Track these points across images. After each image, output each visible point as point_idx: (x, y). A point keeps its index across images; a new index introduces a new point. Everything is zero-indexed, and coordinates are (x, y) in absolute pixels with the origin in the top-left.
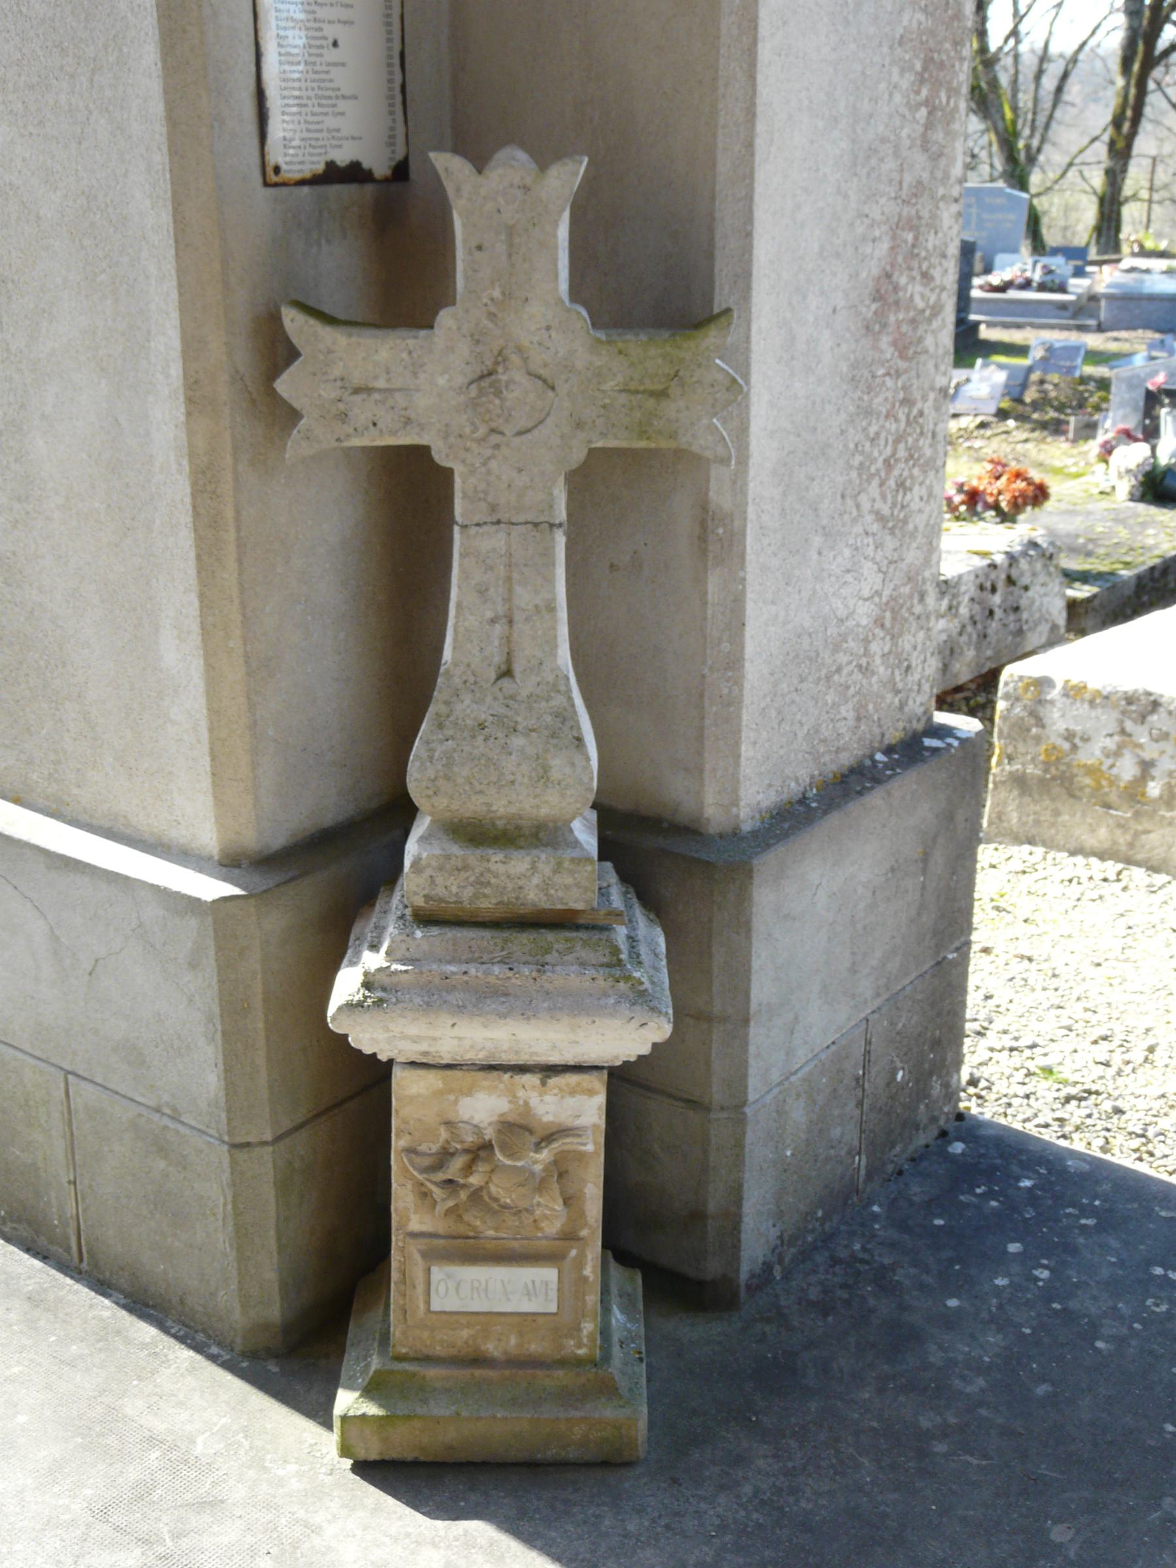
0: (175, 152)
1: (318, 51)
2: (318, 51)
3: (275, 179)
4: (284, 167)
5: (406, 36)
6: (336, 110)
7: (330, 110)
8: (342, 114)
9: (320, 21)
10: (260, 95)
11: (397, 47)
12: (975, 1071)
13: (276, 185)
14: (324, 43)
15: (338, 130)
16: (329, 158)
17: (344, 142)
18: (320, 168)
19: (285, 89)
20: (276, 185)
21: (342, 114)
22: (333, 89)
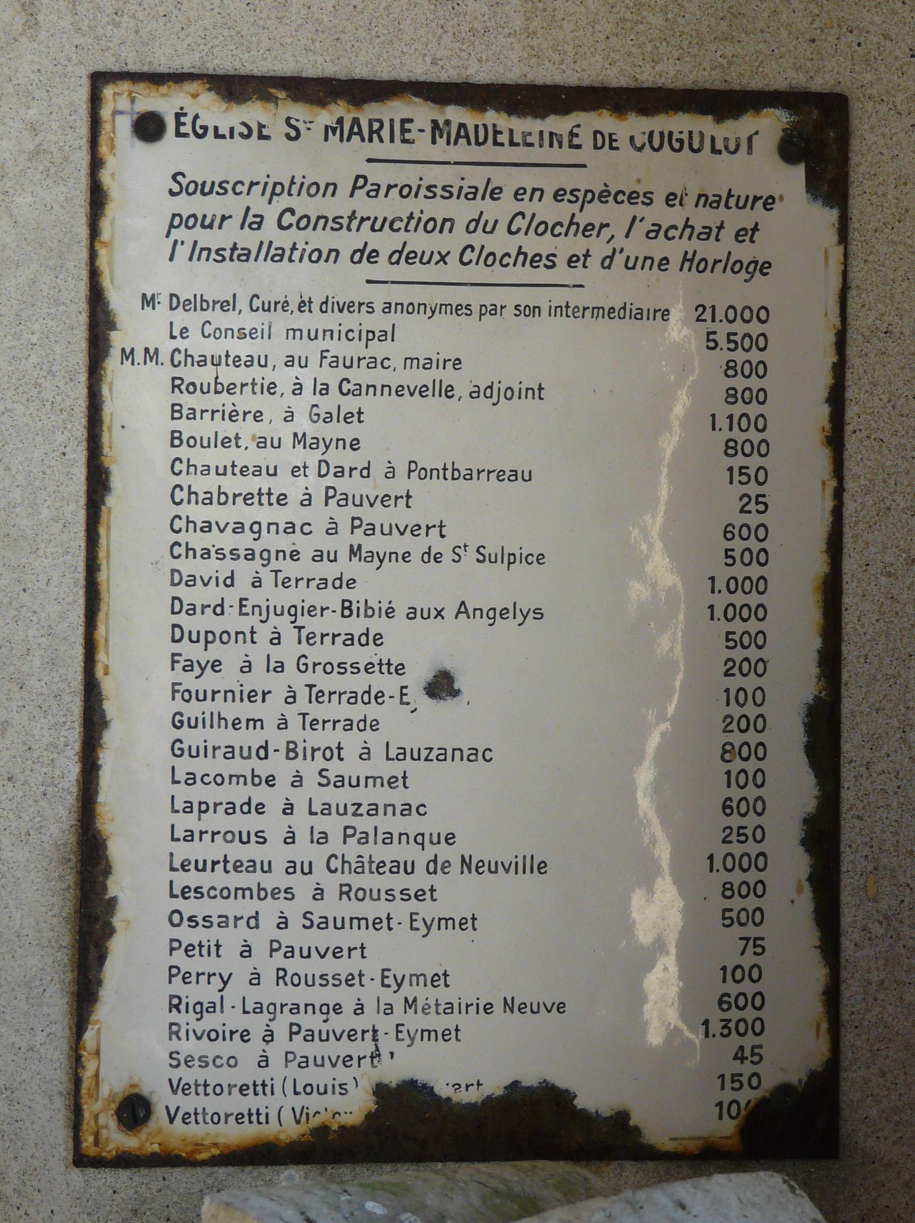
0: (846, 176)
1: (356, 712)
2: (356, 712)
3: (118, 1139)
4: (163, 1099)
5: (850, 652)
6: (427, 910)
7: (400, 910)
8: (467, 923)
9: (369, 611)
10: (90, 856)
11: (792, 682)
12: (97, 1027)
13: (125, 1161)
14: (388, 684)
15: (439, 979)
16: (391, 1073)
17: (467, 1022)
18: (354, 1106)
19: (189, 836)
20: (125, 1161)
21: (467, 923)
22: (420, 840)
